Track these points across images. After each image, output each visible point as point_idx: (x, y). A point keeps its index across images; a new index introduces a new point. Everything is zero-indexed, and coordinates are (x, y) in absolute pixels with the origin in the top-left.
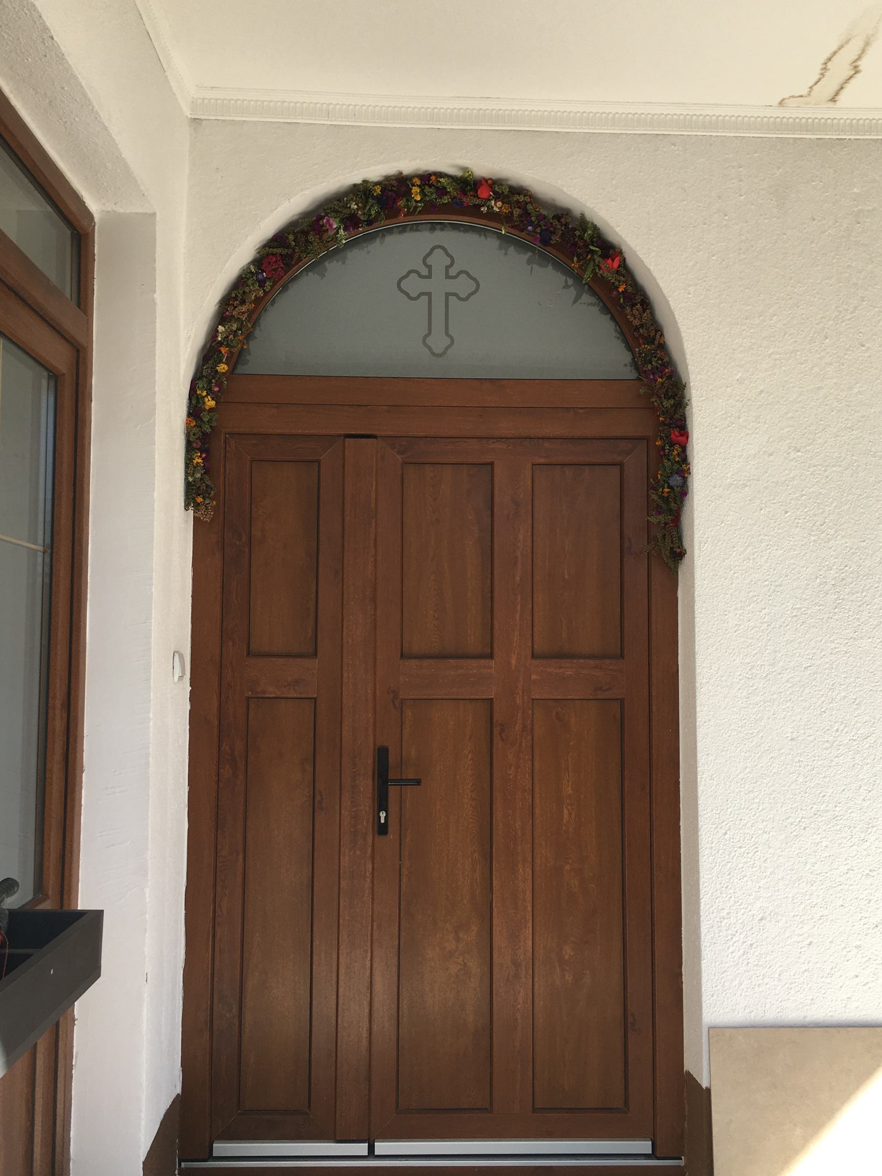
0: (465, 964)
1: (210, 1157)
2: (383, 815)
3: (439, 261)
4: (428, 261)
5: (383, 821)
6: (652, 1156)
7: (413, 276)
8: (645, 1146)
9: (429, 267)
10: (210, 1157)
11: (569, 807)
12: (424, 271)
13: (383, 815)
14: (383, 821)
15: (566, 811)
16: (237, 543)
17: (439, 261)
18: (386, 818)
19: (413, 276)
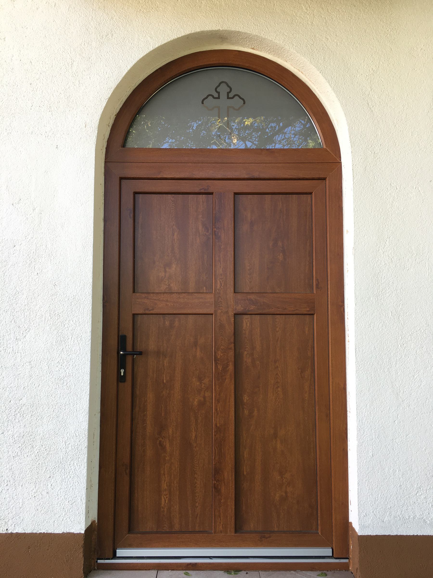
0: (282, 478)
1: (114, 557)
2: (122, 371)
3: (223, 89)
4: (218, 90)
5: (122, 374)
6: (332, 557)
7: (210, 97)
8: (328, 552)
9: (219, 93)
10: (114, 557)
11: (165, 497)
12: (216, 95)
13: (122, 371)
14: (122, 374)
15: (163, 499)
16: (161, 440)
17: (223, 89)
18: (124, 373)
19: (210, 97)
